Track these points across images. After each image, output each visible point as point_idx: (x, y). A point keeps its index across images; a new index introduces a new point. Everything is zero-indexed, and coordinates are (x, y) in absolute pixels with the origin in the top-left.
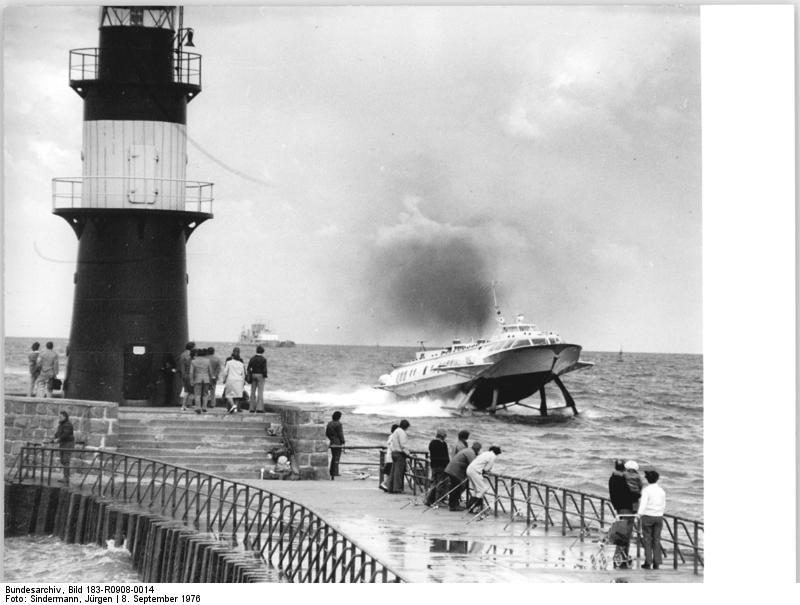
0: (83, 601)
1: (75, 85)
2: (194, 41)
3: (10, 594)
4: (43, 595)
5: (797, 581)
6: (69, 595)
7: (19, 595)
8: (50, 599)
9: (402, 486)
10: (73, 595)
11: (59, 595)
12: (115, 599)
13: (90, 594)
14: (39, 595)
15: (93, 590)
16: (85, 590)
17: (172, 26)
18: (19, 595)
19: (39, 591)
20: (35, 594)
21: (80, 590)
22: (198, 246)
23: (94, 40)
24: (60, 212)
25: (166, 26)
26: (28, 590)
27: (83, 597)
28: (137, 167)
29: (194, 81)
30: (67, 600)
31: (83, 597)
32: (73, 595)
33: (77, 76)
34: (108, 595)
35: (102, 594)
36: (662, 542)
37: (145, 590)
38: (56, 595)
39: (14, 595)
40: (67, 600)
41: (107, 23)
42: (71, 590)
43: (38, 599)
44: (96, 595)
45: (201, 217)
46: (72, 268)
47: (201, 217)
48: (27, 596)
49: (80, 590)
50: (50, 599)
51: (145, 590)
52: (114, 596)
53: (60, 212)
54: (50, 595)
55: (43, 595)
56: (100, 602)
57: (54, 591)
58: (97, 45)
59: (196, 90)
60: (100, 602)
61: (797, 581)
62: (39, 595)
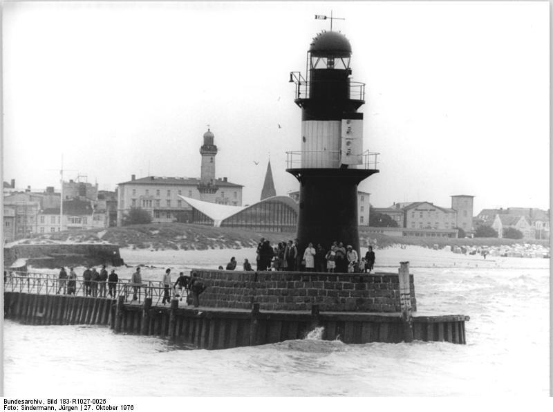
3: (7, 404)
5: (551, 396)
7: (13, 405)
10: (51, 405)
12: (79, 408)
14: (27, 405)
16: (59, 402)
18: (13, 405)
19: (27, 402)
20: (24, 404)
21: (56, 402)
26: (19, 402)
35: (71, 405)
38: (39, 405)
39: (10, 405)
42: (49, 401)
48: (19, 406)
49: (56, 402)
57: (37, 402)
61: (551, 396)
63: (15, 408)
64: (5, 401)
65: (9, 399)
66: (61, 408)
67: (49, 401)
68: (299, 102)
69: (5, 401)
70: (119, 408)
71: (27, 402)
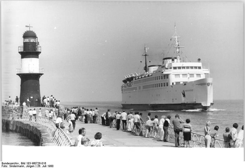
0: (25, 167)
1: (19, 52)
2: (39, 44)
3: (3, 164)
4: (13, 165)
5: (244, 161)
6: (21, 165)
7: (6, 165)
8: (15, 166)
9: (242, 116)
10: (22, 165)
11: (18, 165)
12: (35, 166)
13: (28, 164)
14: (12, 165)
15: (29, 163)
16: (26, 163)
17: (36, 41)
18: (6, 165)
19: (12, 164)
20: (11, 165)
21: (25, 163)
22: (41, 79)
23: (22, 45)
24: (17, 74)
25: (35, 42)
26: (9, 163)
27: (25, 165)
28: (31, 66)
29: (40, 51)
30: (21, 166)
31: (25, 165)
32: (22, 165)
33: (20, 51)
34: (33, 165)
35: (31, 165)
36: (224, 140)
37: (43, 163)
38: (17, 165)
39: (4, 165)
40: (21, 166)
41: (25, 42)
42: (22, 163)
43: (12, 166)
44: (29, 165)
45: (42, 74)
46: (40, 86)
47: (42, 74)
48: (8, 165)
49: (25, 163)
50: (15, 166)
51: (43, 163)
52: (35, 165)
53: (17, 74)
54: (15, 165)
55: (13, 165)
56: (31, 167)
57: (16, 164)
58: (23, 45)
59: (40, 53)
60: (31, 167)
61: (244, 161)
62: (12, 165)
64: (2, 163)
66: (43, 166)
67: (22, 163)
69: (2, 163)
70: (47, 166)
71: (12, 164)
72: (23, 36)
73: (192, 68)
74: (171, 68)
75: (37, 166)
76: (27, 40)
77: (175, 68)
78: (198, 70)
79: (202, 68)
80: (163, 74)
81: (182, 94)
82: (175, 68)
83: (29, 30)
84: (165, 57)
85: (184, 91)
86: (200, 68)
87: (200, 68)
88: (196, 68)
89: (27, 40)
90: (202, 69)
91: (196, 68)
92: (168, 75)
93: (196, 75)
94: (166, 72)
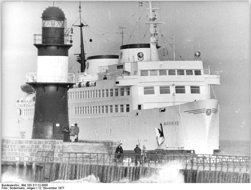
3: (3, 186)
4: (13, 187)
7: (6, 187)
8: (16, 188)
10: (23, 187)
12: (36, 188)
13: (28, 186)
14: (12, 187)
15: (29, 185)
16: (27, 185)
18: (6, 187)
19: (12, 186)
20: (11, 187)
21: (25, 185)
24: (160, 47)
26: (9, 185)
27: (26, 187)
31: (26, 187)
32: (23, 187)
35: (32, 187)
38: (18, 187)
39: (4, 187)
40: (21, 188)
42: (22, 185)
44: (30, 187)
48: (9, 187)
49: (25, 185)
53: (160, 47)
55: (13, 187)
57: (17, 186)
60: (31, 189)
62: (12, 187)
63: (7, 188)
65: (4, 184)
67: (22, 185)
68: (38, 46)
69: (2, 185)
71: (12, 186)
72: (41, 16)
73: (181, 72)
74: (135, 73)
75: (38, 188)
76: (49, 24)
77: (144, 73)
78: (194, 77)
79: (202, 72)
80: (117, 85)
81: (158, 131)
82: (144, 73)
83: (53, 6)
84: (125, 44)
85: (161, 125)
86: (198, 73)
87: (198, 73)
88: (189, 72)
89: (49, 24)
90: (203, 76)
91: (189, 72)
92: (129, 89)
93: (49, 149)
94: (124, 81)
